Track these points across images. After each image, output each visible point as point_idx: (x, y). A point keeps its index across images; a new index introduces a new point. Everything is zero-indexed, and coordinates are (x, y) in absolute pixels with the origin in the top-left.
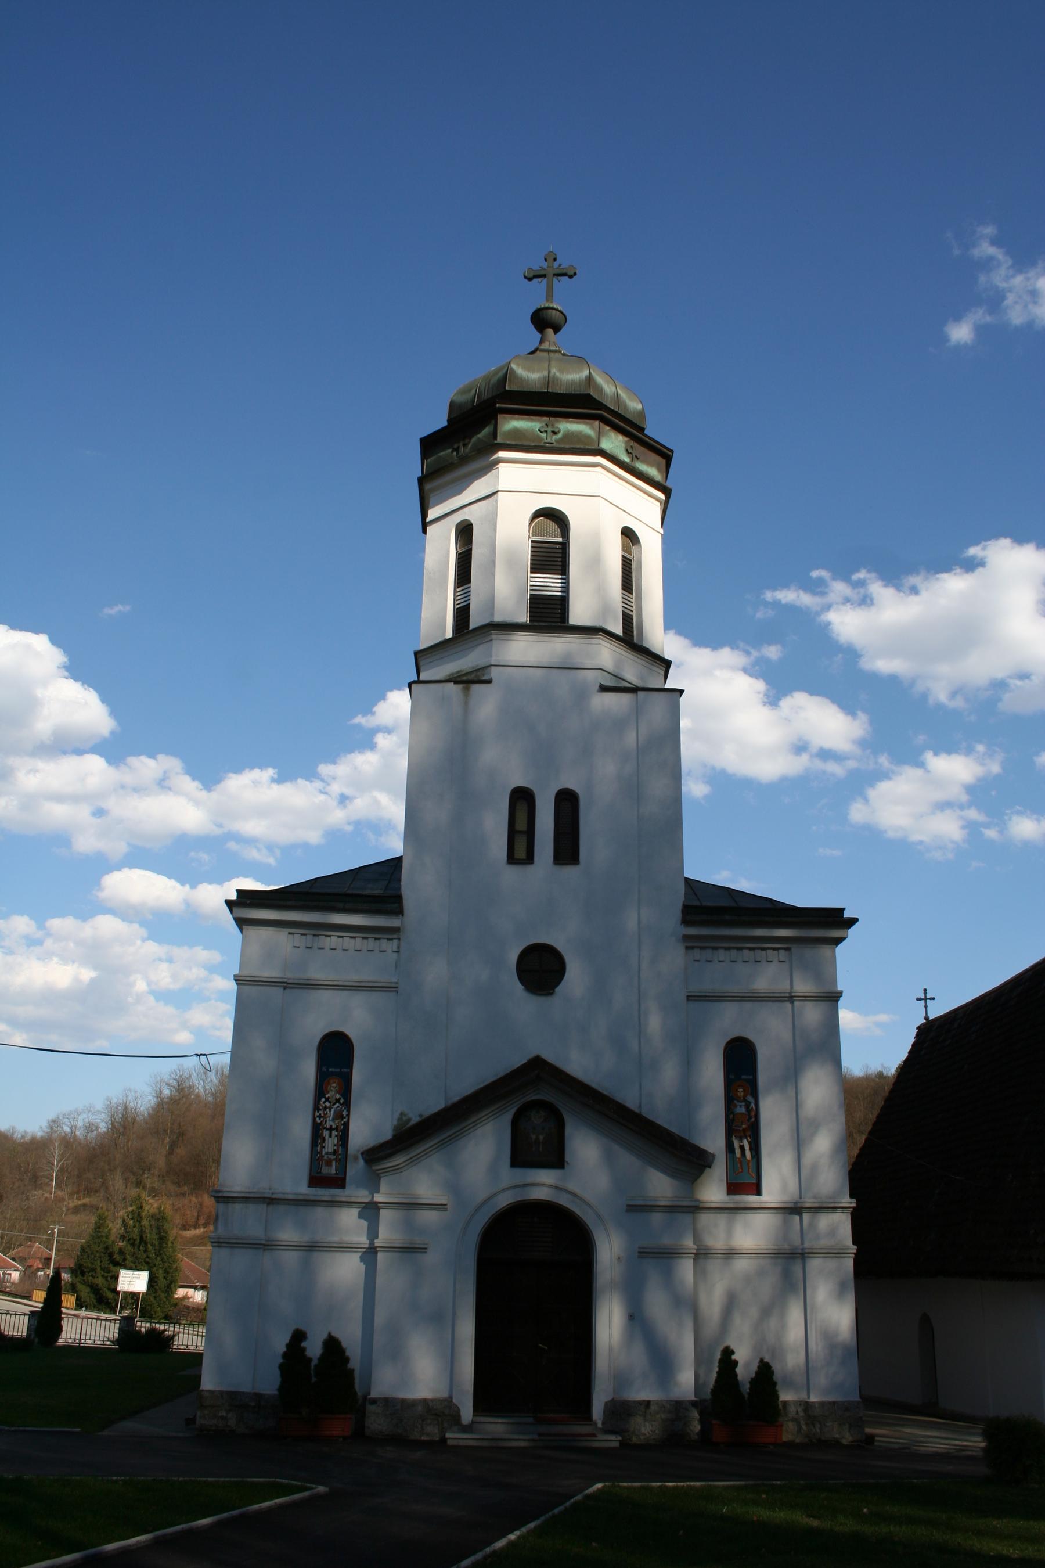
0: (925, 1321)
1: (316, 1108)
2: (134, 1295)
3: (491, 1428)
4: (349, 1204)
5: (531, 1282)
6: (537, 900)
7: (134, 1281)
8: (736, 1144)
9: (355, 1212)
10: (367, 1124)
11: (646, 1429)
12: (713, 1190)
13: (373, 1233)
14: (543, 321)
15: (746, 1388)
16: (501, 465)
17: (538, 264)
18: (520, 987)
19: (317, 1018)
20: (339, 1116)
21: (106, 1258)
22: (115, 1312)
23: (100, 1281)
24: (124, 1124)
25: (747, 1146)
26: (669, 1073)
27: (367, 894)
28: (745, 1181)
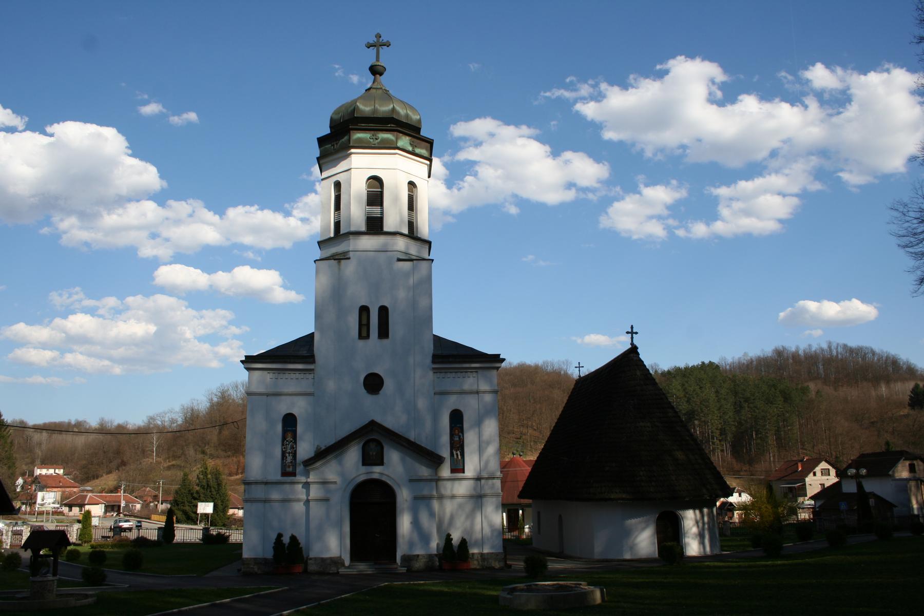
0: (560, 516)
1: (283, 445)
2: (206, 515)
4: (298, 483)
5: (371, 511)
6: (373, 354)
7: (206, 508)
9: (300, 486)
10: (305, 449)
11: (419, 565)
12: (445, 472)
13: (308, 494)
14: (376, 71)
15: (456, 550)
17: (372, 40)
18: (364, 391)
19: (284, 407)
20: (292, 447)
21: (190, 497)
22: (196, 524)
23: (187, 508)
24: (192, 419)
26: (428, 424)
27: (295, 354)
28: (458, 468)
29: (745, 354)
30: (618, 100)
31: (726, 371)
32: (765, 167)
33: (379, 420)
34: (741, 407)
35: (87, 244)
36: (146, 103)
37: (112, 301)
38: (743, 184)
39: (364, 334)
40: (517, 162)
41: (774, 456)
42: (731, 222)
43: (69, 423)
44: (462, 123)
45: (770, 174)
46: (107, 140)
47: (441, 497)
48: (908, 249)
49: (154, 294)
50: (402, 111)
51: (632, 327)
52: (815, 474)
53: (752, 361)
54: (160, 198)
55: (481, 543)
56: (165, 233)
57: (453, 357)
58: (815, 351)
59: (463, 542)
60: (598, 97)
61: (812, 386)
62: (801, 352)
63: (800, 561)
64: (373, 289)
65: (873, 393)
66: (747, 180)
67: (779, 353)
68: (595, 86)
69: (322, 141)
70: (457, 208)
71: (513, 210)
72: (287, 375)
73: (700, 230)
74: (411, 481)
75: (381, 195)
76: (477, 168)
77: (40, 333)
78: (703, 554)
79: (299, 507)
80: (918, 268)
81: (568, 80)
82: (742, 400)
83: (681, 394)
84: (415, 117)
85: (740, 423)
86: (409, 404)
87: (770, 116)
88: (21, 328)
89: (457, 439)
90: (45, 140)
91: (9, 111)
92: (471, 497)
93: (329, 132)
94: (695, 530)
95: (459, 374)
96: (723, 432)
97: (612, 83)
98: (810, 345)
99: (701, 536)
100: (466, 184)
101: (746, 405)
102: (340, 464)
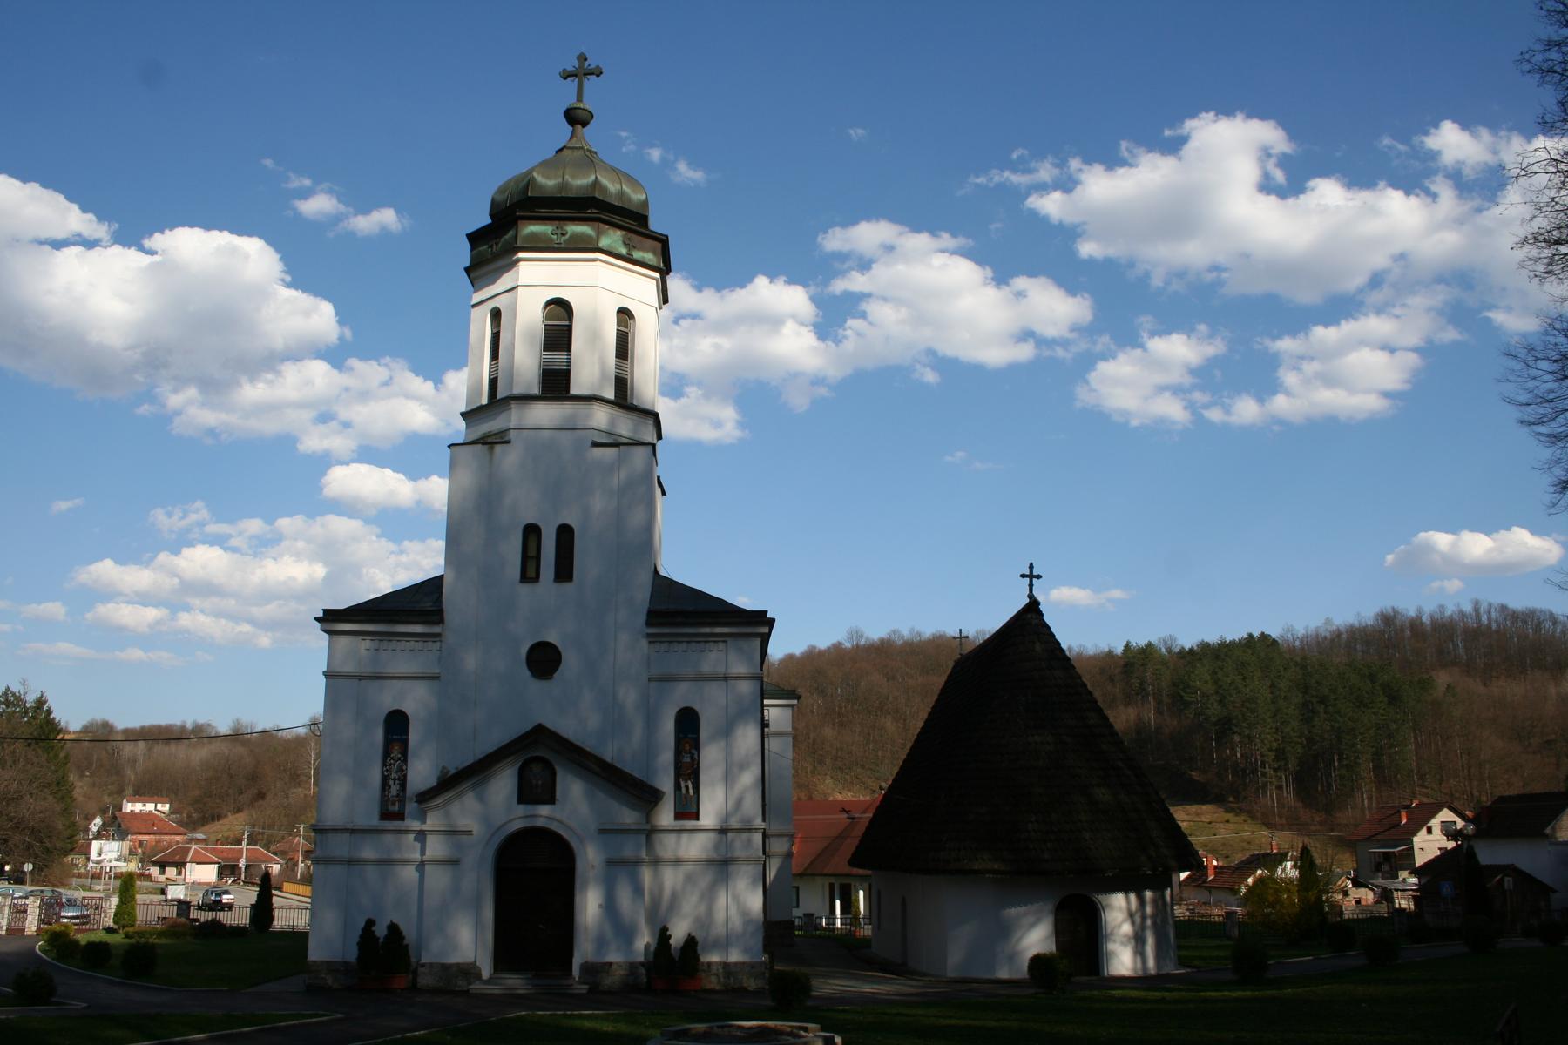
1: (384, 765)
4: (407, 832)
5: (532, 882)
6: (544, 610)
9: (411, 837)
10: (421, 771)
11: (612, 980)
12: (665, 816)
13: (423, 852)
14: (576, 118)
17: (572, 64)
18: (528, 673)
19: (388, 698)
20: (401, 770)
27: (413, 608)
28: (688, 811)
29: (1328, 621)
30: (1102, 188)
31: (1292, 650)
32: (1361, 304)
33: (549, 724)
35: (211, 432)
36: (306, 194)
37: (254, 526)
38: (1319, 332)
39: (531, 573)
40: (941, 295)
41: (1370, 798)
42: (1300, 397)
43: (183, 728)
44: (837, 230)
45: (1366, 315)
46: (253, 258)
47: (656, 862)
48: (1543, 429)
49: (322, 514)
50: (611, 186)
51: (1031, 566)
52: (1429, 831)
53: (1338, 634)
54: (335, 356)
55: (724, 944)
56: (344, 414)
57: (686, 615)
58: (1451, 617)
59: (691, 942)
60: (1067, 185)
61: (1442, 678)
62: (1425, 619)
63: (1274, 992)
64: (556, 493)
65: (1552, 690)
66: (1326, 325)
67: (1388, 619)
68: (1062, 164)
69: (475, 238)
70: (834, 373)
71: (930, 377)
72: (394, 644)
73: (1247, 410)
74: (602, 831)
75: (568, 330)
76: (864, 306)
77: (138, 578)
78: (1140, 973)
79: (409, 874)
80: (1558, 461)
81: (1014, 156)
83: (1210, 688)
84: (638, 197)
87: (1375, 212)
88: (106, 569)
89: (687, 759)
90: (146, 260)
91: (91, 216)
92: (710, 862)
93: (489, 221)
94: (1127, 928)
96: (1280, 755)
97: (1089, 160)
98: (1442, 607)
99: (1138, 940)
100: (849, 332)
101: (1321, 709)
102: (481, 799)
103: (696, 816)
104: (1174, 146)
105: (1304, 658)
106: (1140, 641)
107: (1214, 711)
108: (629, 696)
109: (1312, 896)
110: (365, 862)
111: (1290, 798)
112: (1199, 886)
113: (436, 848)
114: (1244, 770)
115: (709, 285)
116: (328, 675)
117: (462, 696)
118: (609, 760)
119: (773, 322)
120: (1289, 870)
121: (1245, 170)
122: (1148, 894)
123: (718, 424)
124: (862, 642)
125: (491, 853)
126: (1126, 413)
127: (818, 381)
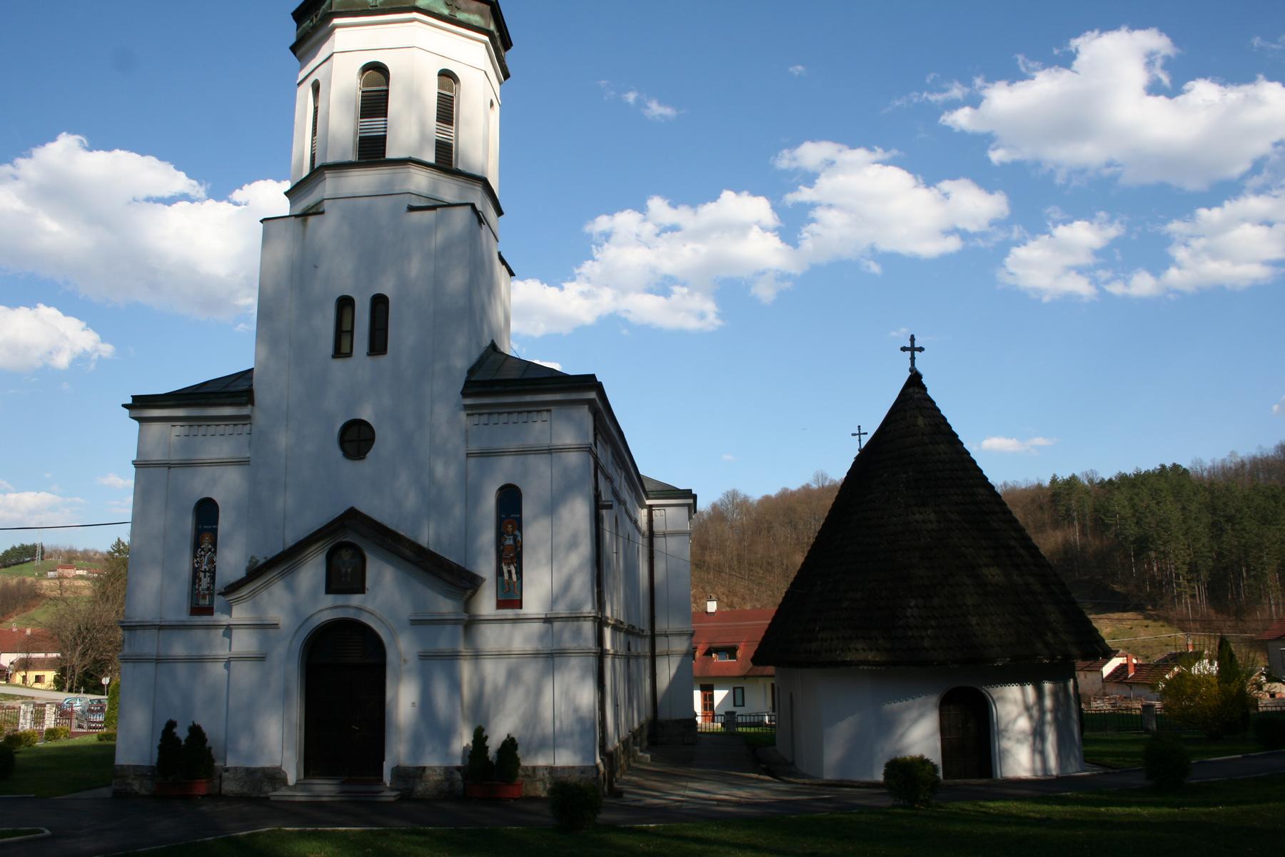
3: (317, 788)
4: (216, 626)
5: (341, 676)
6: (360, 386)
8: (505, 569)
9: (221, 631)
12: (486, 604)
16: (337, 30)
18: (339, 453)
19: (200, 485)
25: (513, 571)
27: (228, 395)
28: (510, 598)
30: (1004, 100)
32: (1244, 187)
33: (363, 508)
34: (1222, 530)
38: (1203, 213)
41: (1277, 605)
42: (1191, 268)
47: (477, 656)
51: (912, 339)
55: (553, 742)
57: (506, 384)
59: (510, 745)
60: (974, 101)
66: (1209, 208)
71: (875, 268)
72: (212, 430)
73: (1143, 284)
74: (415, 622)
76: (812, 214)
78: (1040, 773)
82: (1222, 520)
83: (1128, 512)
85: (1220, 555)
86: (426, 478)
89: (509, 542)
92: (536, 655)
94: (1023, 724)
95: (515, 417)
96: (1193, 568)
99: (1038, 734)
101: (1228, 527)
102: (291, 588)
103: (518, 604)
104: (1067, 60)
105: (1212, 484)
106: (1064, 475)
107: (1132, 531)
108: (445, 472)
109: (1234, 687)
110: (176, 660)
111: (1204, 608)
112: (1120, 682)
113: (243, 642)
114: (1160, 582)
115: (683, 203)
116: (137, 464)
117: (274, 484)
118: (425, 545)
119: (741, 229)
120: (1206, 667)
121: (1134, 75)
122: (1047, 686)
123: (702, 316)
124: (827, 484)
125: (298, 645)
126: (1038, 291)
127: (782, 276)
